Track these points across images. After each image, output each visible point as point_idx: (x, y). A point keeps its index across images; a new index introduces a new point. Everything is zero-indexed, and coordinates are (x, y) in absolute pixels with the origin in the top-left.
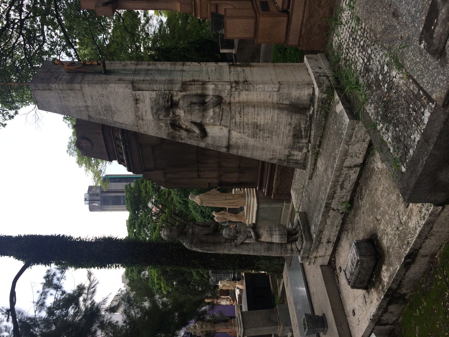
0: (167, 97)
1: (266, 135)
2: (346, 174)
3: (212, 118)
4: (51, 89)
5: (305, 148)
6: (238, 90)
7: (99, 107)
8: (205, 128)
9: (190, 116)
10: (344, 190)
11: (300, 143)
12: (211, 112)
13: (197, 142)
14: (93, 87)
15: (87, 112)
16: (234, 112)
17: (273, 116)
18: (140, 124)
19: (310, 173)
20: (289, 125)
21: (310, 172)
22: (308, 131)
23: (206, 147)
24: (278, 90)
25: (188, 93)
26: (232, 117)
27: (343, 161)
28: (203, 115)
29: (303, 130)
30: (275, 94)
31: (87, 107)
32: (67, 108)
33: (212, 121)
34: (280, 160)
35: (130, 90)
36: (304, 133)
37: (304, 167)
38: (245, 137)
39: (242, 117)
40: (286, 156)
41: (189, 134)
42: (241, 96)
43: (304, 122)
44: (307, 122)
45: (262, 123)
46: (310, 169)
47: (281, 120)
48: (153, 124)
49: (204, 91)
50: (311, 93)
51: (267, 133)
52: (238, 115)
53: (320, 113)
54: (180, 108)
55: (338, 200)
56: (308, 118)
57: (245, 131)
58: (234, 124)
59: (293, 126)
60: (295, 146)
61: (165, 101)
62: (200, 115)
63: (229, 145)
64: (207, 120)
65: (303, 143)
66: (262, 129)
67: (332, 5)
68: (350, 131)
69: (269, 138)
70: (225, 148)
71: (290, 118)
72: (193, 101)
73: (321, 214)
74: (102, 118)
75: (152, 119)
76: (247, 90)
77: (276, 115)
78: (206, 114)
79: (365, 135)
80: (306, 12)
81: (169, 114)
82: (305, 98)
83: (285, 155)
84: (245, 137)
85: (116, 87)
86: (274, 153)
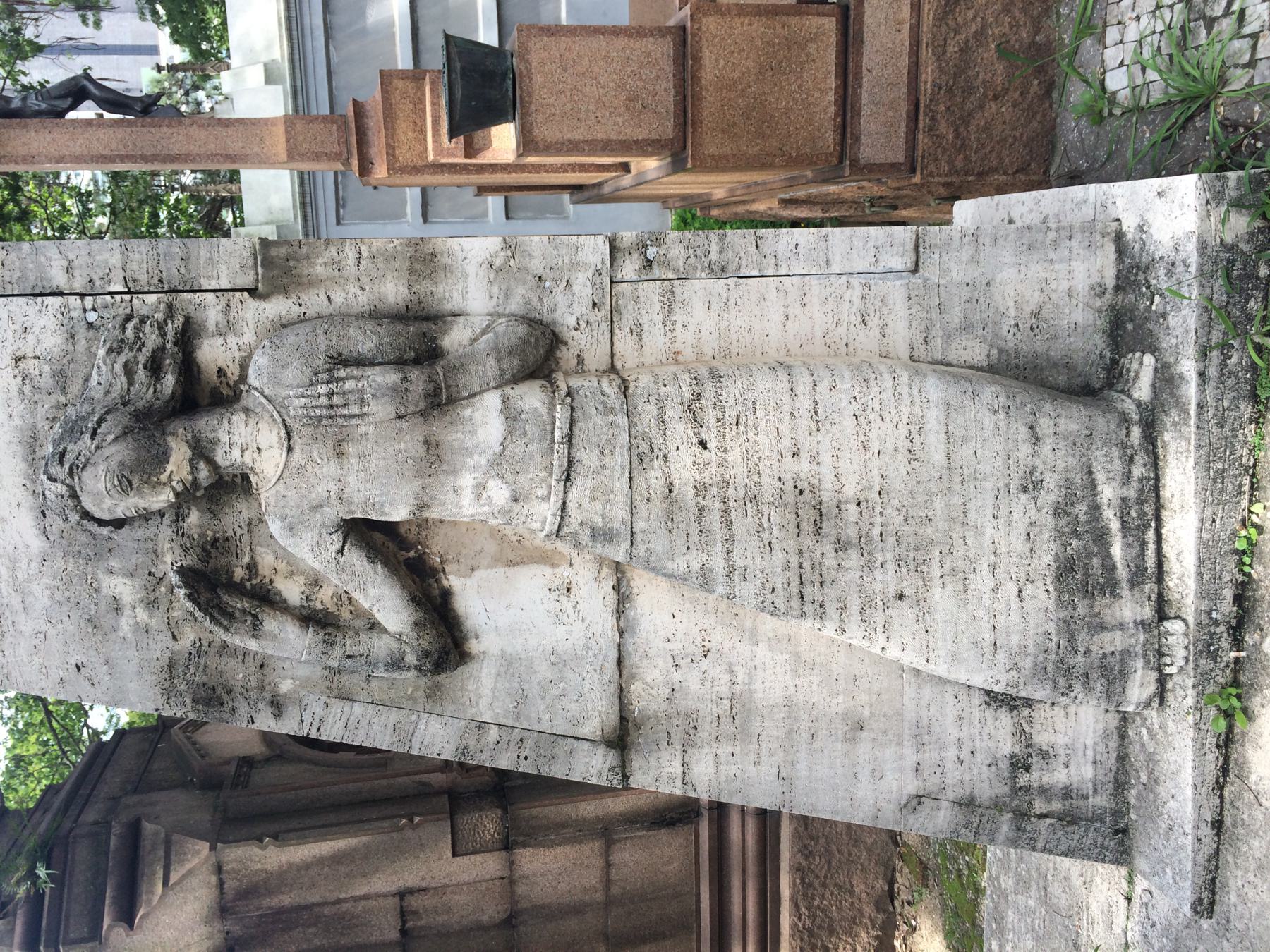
0: (152, 339)
1: (886, 580)
3: (499, 465)
5: (1139, 663)
6: (656, 272)
8: (447, 594)
9: (330, 468)
11: (1103, 628)
13: (393, 716)
16: (650, 410)
19: (1201, 859)
20: (1025, 490)
21: (1196, 852)
22: (1146, 526)
23: (465, 751)
24: (909, 262)
25: (315, 301)
26: (644, 447)
29: (1115, 525)
30: (896, 290)
33: (499, 493)
39: (712, 445)
40: (1004, 765)
41: (329, 643)
42: (679, 317)
43: (1117, 464)
44: (1131, 460)
45: (851, 491)
46: (1197, 827)
47: (968, 451)
48: (41, 596)
49: (423, 287)
51: (890, 566)
52: (680, 430)
53: (1223, 364)
54: (246, 410)
56: (1136, 431)
57: (740, 562)
58: (658, 507)
59: (1052, 497)
61: (129, 370)
62: (410, 441)
63: (623, 719)
64: (457, 491)
65: (1121, 627)
66: (852, 532)
69: (904, 604)
70: (601, 751)
71: (1023, 432)
72: (347, 347)
75: (37, 544)
76: (719, 271)
77: (934, 417)
83: (993, 764)
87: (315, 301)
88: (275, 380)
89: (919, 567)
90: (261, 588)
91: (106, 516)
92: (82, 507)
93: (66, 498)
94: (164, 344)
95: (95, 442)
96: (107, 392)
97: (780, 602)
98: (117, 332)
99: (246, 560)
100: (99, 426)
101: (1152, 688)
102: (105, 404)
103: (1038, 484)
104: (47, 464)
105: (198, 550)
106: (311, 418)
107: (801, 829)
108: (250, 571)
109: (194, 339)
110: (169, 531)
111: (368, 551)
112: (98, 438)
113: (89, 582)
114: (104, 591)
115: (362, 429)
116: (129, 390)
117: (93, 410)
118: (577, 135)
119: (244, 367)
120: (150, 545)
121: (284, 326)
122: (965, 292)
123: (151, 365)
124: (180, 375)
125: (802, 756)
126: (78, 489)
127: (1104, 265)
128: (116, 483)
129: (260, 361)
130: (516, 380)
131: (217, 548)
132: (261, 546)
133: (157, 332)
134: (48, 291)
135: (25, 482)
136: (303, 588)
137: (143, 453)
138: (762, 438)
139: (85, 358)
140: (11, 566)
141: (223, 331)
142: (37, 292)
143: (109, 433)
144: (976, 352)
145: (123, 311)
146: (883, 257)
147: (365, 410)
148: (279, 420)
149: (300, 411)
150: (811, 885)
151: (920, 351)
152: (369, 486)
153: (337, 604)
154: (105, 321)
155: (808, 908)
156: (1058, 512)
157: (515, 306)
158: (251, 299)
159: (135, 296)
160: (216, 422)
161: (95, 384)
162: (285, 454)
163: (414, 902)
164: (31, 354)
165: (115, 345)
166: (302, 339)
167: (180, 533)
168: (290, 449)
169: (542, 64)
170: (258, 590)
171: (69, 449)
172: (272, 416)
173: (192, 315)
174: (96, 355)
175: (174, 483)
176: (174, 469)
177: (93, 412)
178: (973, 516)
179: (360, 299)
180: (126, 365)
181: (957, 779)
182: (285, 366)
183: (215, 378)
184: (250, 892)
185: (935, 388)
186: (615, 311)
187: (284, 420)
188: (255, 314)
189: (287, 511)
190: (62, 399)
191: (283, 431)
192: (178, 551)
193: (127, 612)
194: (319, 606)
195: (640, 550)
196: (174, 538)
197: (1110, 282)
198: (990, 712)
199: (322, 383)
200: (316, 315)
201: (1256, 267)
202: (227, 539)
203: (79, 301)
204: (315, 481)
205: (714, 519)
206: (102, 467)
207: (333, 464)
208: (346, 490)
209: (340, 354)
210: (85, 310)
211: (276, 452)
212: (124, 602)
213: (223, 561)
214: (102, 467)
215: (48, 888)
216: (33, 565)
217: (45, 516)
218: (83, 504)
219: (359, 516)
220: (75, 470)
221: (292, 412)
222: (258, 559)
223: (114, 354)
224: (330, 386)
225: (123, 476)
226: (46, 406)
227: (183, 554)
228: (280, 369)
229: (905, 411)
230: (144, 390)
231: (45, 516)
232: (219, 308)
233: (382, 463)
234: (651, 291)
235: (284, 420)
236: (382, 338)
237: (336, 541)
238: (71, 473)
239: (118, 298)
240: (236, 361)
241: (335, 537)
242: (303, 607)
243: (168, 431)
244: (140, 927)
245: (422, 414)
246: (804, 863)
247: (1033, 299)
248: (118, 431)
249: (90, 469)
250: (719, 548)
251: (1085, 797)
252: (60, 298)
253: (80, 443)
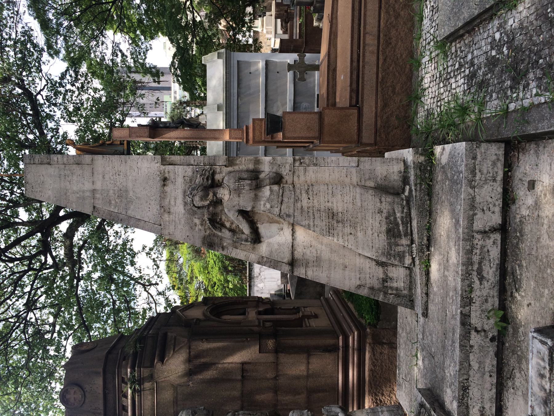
0: (207, 174)
1: (348, 230)
2: (483, 247)
3: (269, 200)
4: (52, 163)
5: (407, 254)
6: (303, 165)
7: (111, 192)
8: (257, 228)
9: (237, 199)
10: (486, 283)
11: (398, 245)
12: (266, 191)
13: (245, 253)
14: (108, 159)
15: (92, 201)
16: (299, 191)
17: (354, 198)
18: (164, 220)
19: (423, 302)
20: (379, 213)
21: (422, 300)
24: (356, 164)
25: (236, 168)
26: (297, 198)
27: (471, 220)
29: (400, 222)
30: (354, 170)
31: (94, 191)
32: (66, 194)
33: (268, 206)
34: (372, 288)
35: (158, 165)
36: (403, 227)
37: (411, 304)
38: (316, 245)
39: (311, 199)
40: (381, 280)
41: (234, 235)
42: (307, 174)
43: (400, 209)
44: (404, 208)
45: (340, 210)
46: (421, 294)
47: (366, 204)
48: (183, 222)
49: (257, 166)
50: (402, 169)
51: (349, 227)
52: (304, 195)
53: (420, 188)
55: (480, 307)
56: (405, 202)
57: (316, 223)
58: (300, 211)
59: (385, 215)
60: (393, 252)
61: (203, 179)
63: (293, 259)
64: (260, 205)
65: (403, 245)
66: (340, 219)
67: (408, 91)
68: (471, 161)
70: (288, 266)
71: (378, 200)
73: (457, 345)
74: (112, 210)
75: (183, 211)
76: (315, 165)
77: (358, 196)
78: (260, 194)
79: (493, 168)
80: (379, 100)
81: (208, 195)
82: (396, 178)
84: (316, 245)
85: (140, 160)
86: (362, 276)
87: (236, 168)
88: (229, 182)
89: (355, 228)
97: (324, 233)
101: (411, 261)
103: (382, 212)
107: (372, 356)
118: (295, 136)
119: (223, 180)
122: (369, 171)
125: (332, 272)
127: (401, 167)
129: (226, 178)
130: (274, 184)
138: (321, 198)
144: (372, 184)
146: (351, 163)
150: (375, 377)
151: (359, 183)
155: (375, 385)
156: (387, 218)
157: (274, 170)
163: (246, 367)
169: (288, 120)
178: (367, 218)
181: (369, 282)
184: (197, 356)
185: (358, 190)
186: (294, 172)
188: (226, 170)
195: (296, 219)
197: (403, 171)
198: (377, 267)
201: (427, 167)
205: (311, 214)
215: (139, 350)
229: (352, 194)
234: (301, 168)
244: (165, 363)
245: (254, 189)
246: (373, 368)
247: (385, 173)
250: (312, 220)
251: (402, 291)
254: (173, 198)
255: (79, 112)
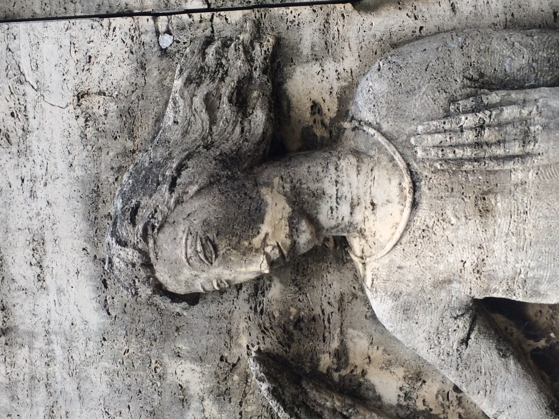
28: (528, 102)
54: (357, 153)
90: (351, 380)
91: (181, 290)
92: (156, 279)
93: (138, 266)
94: (251, 71)
95: (175, 195)
96: (185, 133)
98: (196, 59)
99: (335, 345)
100: (179, 175)
102: (185, 146)
104: (115, 224)
105: (279, 331)
106: (447, 161)
108: (339, 359)
109: (285, 65)
110: (246, 307)
111: (498, 341)
112: (178, 190)
113: (153, 366)
114: (170, 378)
115: (516, 177)
116: (211, 129)
117: (170, 154)
120: (224, 324)
121: (394, 46)
123: (237, 99)
124: (270, 110)
126: (152, 256)
128: (199, 248)
131: (301, 329)
132: (354, 328)
133: (243, 57)
134: (116, 11)
135: (85, 245)
136: (401, 383)
137: (233, 209)
139: (157, 93)
140: (67, 346)
141: (320, 54)
142: (103, 12)
143: (191, 183)
145: (201, 33)
147: (529, 148)
148: (402, 164)
149: (433, 152)
152: (521, 255)
153: (442, 405)
154: (181, 45)
158: (355, 12)
159: (216, 14)
160: (320, 169)
161: (170, 123)
162: (407, 210)
164: (95, 90)
165: (194, 74)
166: (432, 57)
167: (259, 309)
168: (415, 205)
170: (347, 382)
171: (143, 203)
172: (392, 159)
173: (283, 35)
174: (169, 90)
175: (268, 249)
176: (270, 231)
177: (170, 157)
179: (493, 6)
180: (207, 99)
182: (410, 93)
183: (308, 115)
187: (408, 165)
189: (403, 287)
190: (130, 144)
191: (407, 182)
192: (256, 332)
193: (195, 404)
194: (420, 406)
196: (252, 315)
199: (465, 113)
200: (436, 30)
202: (314, 319)
203: (151, 22)
204: (444, 248)
206: (182, 228)
207: (474, 224)
208: (489, 261)
209: (482, 75)
210: (158, 33)
211: (395, 208)
212: (192, 392)
213: (308, 345)
214: (182, 228)
216: (91, 344)
217: (106, 287)
218: (157, 275)
219: (499, 295)
220: (150, 232)
221: (420, 154)
222: (350, 345)
223: (193, 86)
224: (480, 115)
225: (208, 239)
226: (111, 154)
227: (261, 336)
228: (403, 97)
230: (230, 129)
231: (106, 287)
232: (316, 25)
233: (542, 223)
235: (408, 165)
236: (537, 52)
237: (463, 324)
238: (145, 236)
239: (196, 16)
240: (334, 93)
241: (460, 323)
242: (400, 406)
243: (261, 180)
248: (202, 180)
249: (168, 229)
252: (130, 19)
253: (156, 196)
254: (22, 239)
255: (416, 317)
